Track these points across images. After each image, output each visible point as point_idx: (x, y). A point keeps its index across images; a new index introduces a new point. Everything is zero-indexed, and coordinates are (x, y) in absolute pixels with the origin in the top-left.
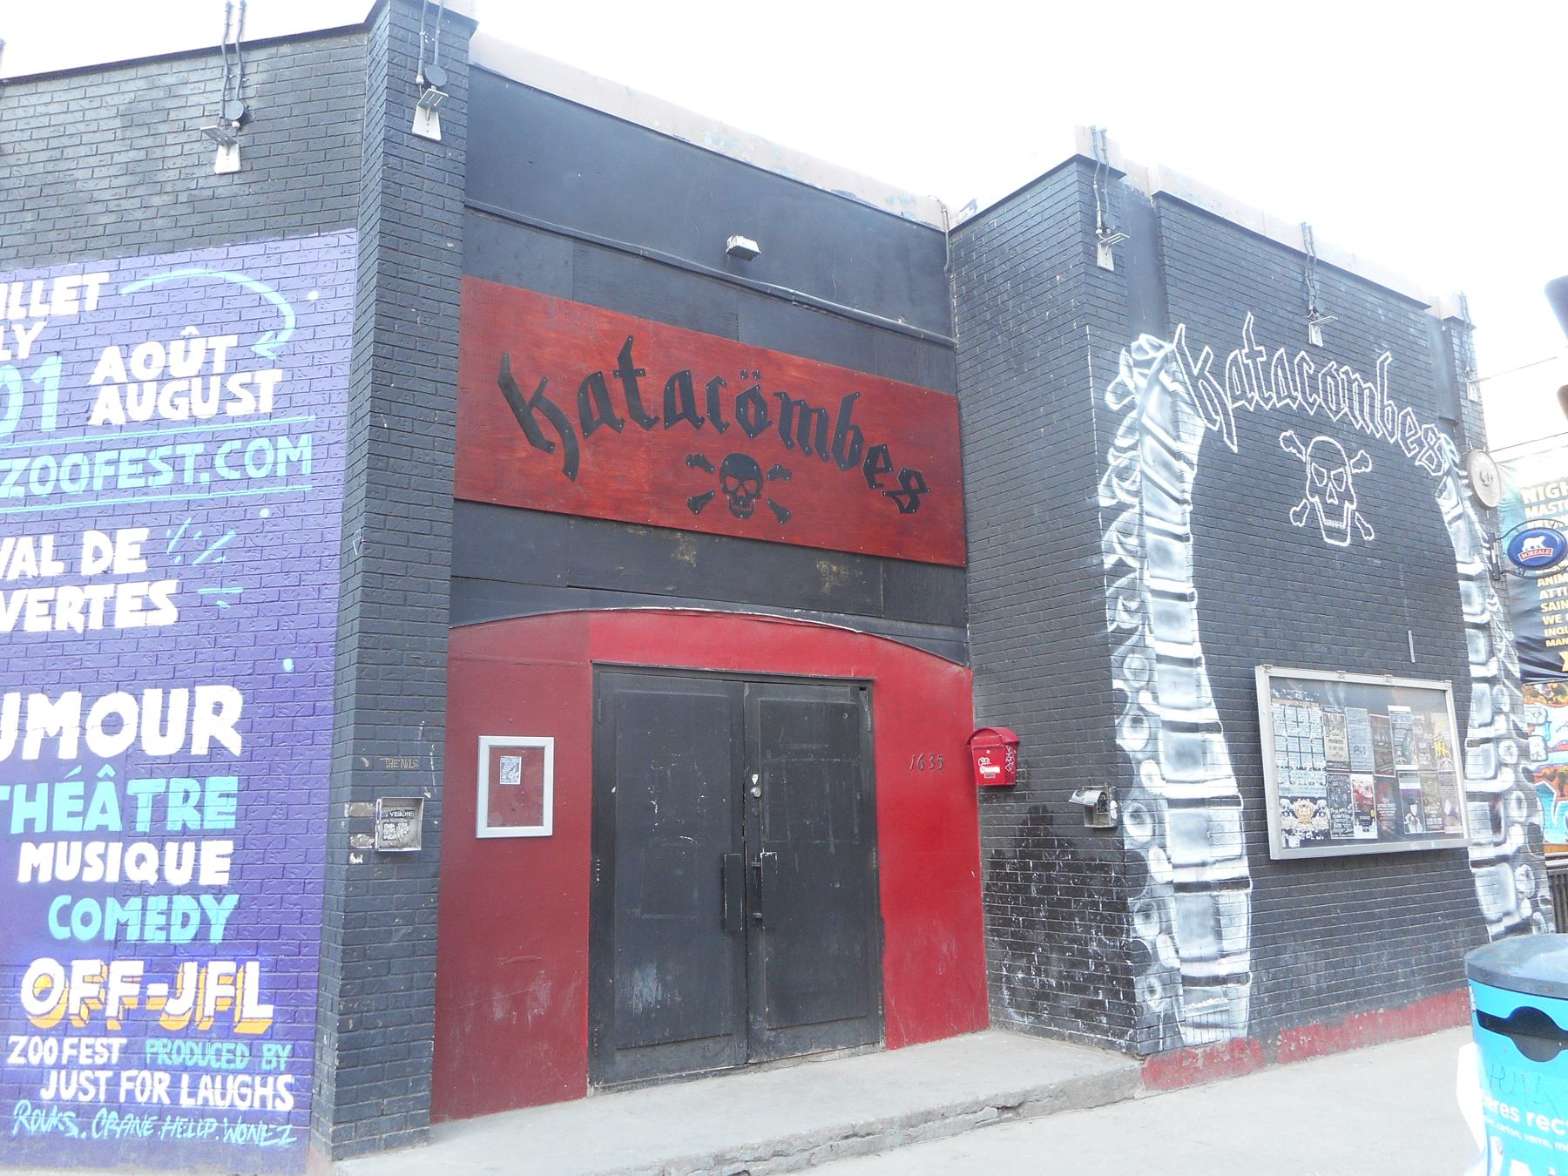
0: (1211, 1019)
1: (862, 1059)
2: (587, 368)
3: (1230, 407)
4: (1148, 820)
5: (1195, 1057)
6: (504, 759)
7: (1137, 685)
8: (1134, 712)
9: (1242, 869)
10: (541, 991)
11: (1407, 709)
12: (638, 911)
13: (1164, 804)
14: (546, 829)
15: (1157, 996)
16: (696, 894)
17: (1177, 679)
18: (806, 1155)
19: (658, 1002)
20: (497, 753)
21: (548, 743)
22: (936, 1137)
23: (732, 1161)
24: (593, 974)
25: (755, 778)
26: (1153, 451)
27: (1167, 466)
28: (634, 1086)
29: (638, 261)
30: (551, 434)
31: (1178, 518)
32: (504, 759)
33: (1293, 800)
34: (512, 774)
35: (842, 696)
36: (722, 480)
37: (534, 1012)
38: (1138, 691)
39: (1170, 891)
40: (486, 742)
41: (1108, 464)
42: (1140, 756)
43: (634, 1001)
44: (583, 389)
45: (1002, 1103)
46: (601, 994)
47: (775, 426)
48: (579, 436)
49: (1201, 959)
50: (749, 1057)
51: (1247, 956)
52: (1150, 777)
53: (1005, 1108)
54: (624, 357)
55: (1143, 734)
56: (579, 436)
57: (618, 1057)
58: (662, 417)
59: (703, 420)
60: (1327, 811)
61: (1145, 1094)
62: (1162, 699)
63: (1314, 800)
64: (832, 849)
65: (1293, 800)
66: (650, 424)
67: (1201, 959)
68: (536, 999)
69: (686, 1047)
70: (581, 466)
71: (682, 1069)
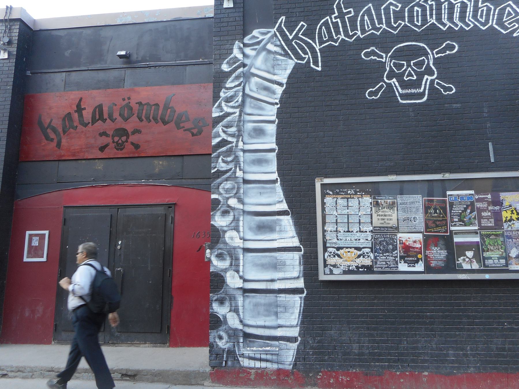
0: (263, 356)
2: (67, 112)
3: (317, 48)
4: (228, 258)
5: (249, 373)
6: (34, 238)
7: (227, 196)
8: (224, 208)
9: (300, 284)
10: (40, 309)
11: (472, 192)
13: (240, 252)
14: (44, 259)
15: (224, 341)
17: (262, 191)
18: (31, 374)
20: (31, 236)
21: (47, 232)
25: (120, 242)
26: (256, 83)
27: (266, 89)
29: (205, 66)
30: (52, 135)
31: (271, 113)
32: (34, 238)
33: (338, 249)
34: (35, 242)
35: (160, 211)
36: (113, 139)
38: (228, 198)
39: (240, 292)
40: (28, 233)
41: (220, 97)
42: (225, 229)
44: (64, 119)
45: (124, 372)
47: (135, 115)
48: (62, 135)
49: (264, 327)
51: (298, 329)
52: (232, 238)
53: (126, 375)
54: (79, 106)
55: (229, 218)
56: (62, 135)
58: (91, 122)
59: (106, 119)
60: (372, 255)
61: (211, 384)
62: (247, 200)
63: (358, 249)
64: (149, 269)
65: (338, 249)
66: (86, 125)
67: (264, 327)
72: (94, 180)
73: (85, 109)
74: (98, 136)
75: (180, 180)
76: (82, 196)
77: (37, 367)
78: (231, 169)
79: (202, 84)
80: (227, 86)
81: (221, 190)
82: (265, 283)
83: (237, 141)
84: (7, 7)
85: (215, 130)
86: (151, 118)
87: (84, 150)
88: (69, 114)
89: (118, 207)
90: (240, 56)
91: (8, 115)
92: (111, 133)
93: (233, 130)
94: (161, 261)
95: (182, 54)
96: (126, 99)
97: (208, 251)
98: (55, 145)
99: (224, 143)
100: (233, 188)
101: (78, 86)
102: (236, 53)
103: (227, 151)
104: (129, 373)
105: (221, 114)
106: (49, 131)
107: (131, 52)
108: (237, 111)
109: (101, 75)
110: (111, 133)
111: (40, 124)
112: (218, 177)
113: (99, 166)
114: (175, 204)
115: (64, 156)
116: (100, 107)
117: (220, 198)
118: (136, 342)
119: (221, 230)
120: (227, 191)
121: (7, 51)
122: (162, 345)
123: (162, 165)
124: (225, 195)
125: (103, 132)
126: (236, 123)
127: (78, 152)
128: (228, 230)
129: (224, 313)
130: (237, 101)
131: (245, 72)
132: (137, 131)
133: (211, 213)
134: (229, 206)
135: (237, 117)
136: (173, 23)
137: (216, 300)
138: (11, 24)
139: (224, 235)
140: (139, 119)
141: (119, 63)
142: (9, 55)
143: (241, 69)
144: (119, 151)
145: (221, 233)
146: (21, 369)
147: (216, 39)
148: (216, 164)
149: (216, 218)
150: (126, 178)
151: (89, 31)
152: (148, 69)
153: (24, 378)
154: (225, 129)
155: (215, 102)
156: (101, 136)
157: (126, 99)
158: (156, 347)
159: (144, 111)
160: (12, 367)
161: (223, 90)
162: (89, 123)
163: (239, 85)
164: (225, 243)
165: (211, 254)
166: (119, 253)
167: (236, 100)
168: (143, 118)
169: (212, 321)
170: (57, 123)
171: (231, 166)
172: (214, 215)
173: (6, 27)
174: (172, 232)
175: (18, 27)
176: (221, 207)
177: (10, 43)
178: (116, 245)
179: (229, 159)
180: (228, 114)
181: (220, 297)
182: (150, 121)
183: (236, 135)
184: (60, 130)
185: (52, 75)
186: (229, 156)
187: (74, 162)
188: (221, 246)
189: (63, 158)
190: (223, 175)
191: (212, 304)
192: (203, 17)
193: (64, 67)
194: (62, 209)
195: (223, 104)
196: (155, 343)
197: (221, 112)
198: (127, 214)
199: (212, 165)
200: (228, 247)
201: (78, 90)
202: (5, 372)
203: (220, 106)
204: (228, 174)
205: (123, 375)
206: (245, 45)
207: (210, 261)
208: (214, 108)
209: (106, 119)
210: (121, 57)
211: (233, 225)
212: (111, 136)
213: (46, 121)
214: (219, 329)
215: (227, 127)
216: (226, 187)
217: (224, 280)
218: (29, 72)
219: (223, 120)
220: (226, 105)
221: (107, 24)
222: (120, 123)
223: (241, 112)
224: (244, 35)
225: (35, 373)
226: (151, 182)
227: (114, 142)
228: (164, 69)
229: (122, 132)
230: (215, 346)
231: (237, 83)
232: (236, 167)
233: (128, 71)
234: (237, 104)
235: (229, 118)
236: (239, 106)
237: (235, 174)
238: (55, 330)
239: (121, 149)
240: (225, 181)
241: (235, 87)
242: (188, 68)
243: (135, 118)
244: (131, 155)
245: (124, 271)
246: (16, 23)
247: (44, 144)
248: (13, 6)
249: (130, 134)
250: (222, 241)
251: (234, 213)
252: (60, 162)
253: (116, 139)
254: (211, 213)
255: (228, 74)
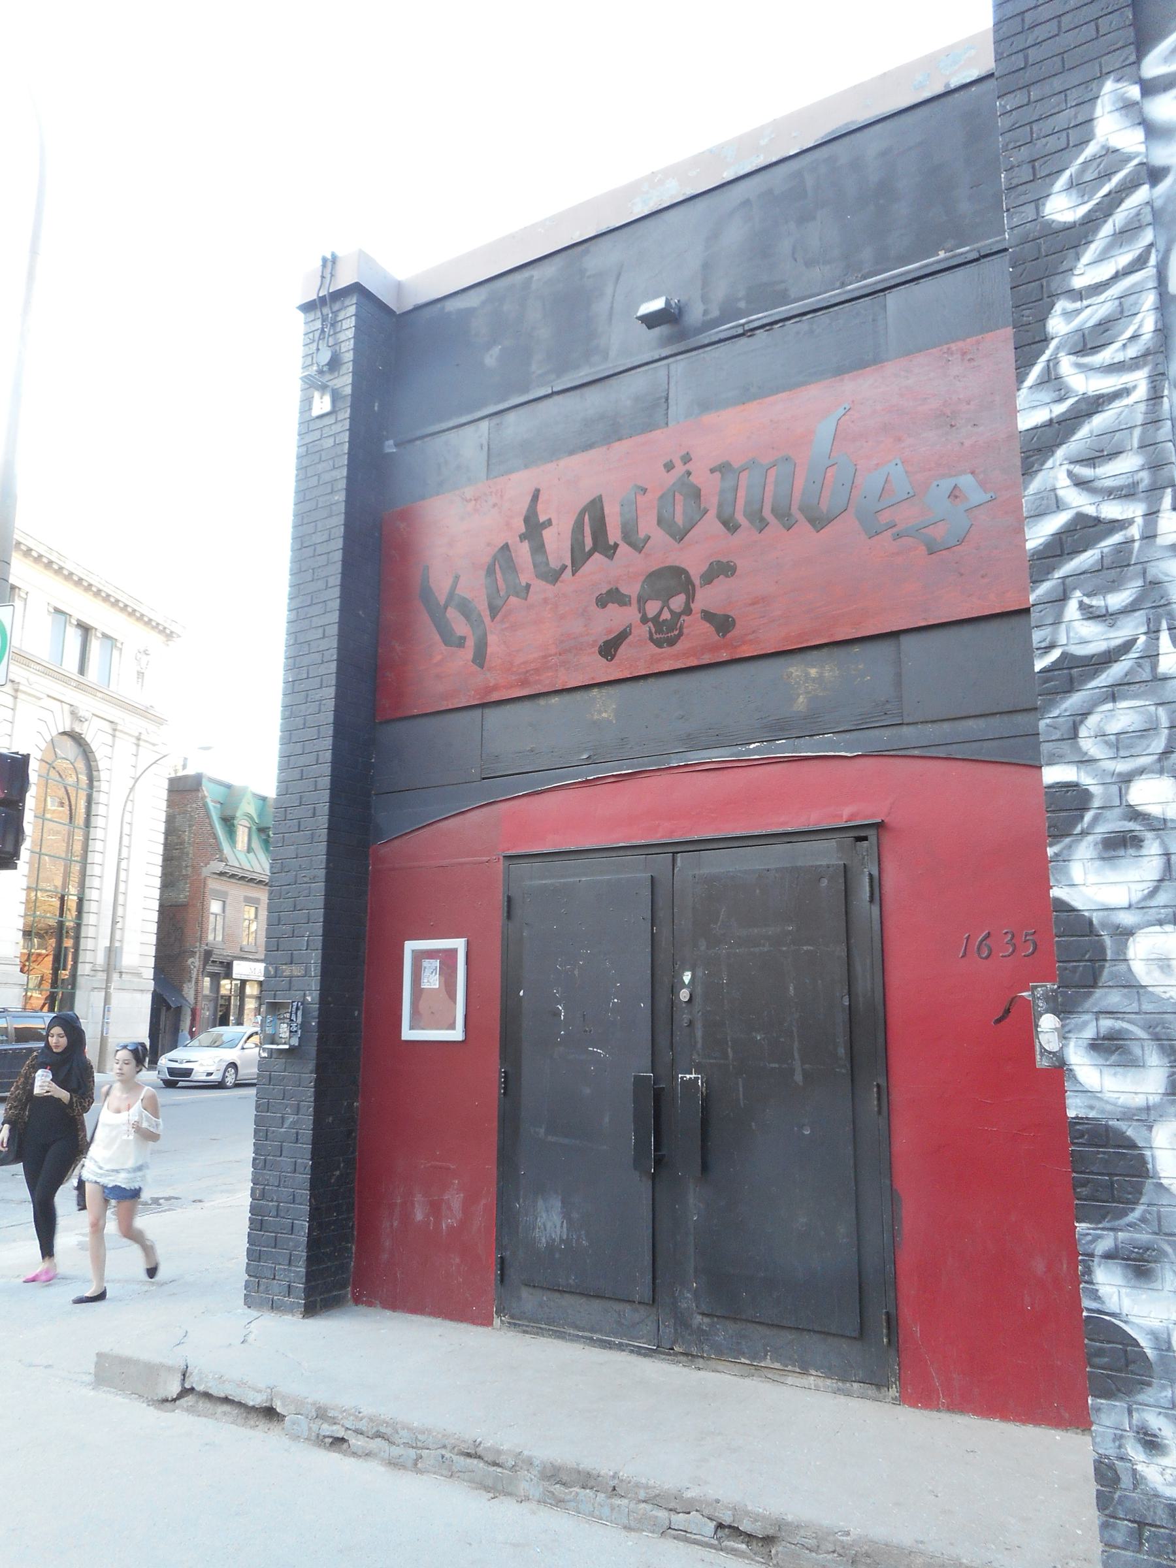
1: (854, 1404)
6: (426, 963)
7: (1122, 767)
8: (1113, 824)
10: (455, 1200)
12: (542, 1131)
14: (457, 1034)
16: (607, 1120)
18: (412, 1453)
19: (562, 1240)
20: (419, 956)
22: (594, 1516)
23: (334, 1421)
24: (501, 1195)
25: (687, 977)
28: (540, 1332)
29: (960, 273)
30: (461, 627)
32: (426, 963)
34: (432, 980)
36: (642, 609)
37: (447, 1222)
38: (1126, 779)
40: (410, 946)
42: (1127, 919)
43: (537, 1234)
44: (490, 571)
45: (727, 1519)
46: (507, 1220)
50: (674, 1342)
53: (735, 1531)
57: (525, 1293)
58: (568, 563)
59: (616, 546)
64: (798, 1078)
66: (554, 576)
68: (449, 1208)
69: (597, 1304)
70: (489, 650)
71: (593, 1330)
72: (590, 761)
73: (549, 523)
74: (593, 607)
75: (894, 730)
76: (563, 818)
77: (429, 1431)
78: (1128, 646)
79: (953, 347)
80: (1078, 282)
81: (1088, 745)
82: (780, 848)
83: (1152, 515)
84: (325, 260)
85: (1036, 484)
86: (767, 513)
87: (554, 660)
88: (506, 547)
89: (675, 849)
90: (1131, 140)
91: (338, 582)
92: (632, 589)
93: (1127, 465)
94: (842, 1051)
95: (867, 254)
96: (678, 463)
97: (1048, 1022)
98: (470, 656)
99: (1085, 530)
100: (1148, 731)
101: (532, 453)
102: (1111, 129)
103: (1101, 568)
104: (746, 1526)
105: (1060, 409)
106: (452, 614)
107: (684, 299)
108: (1139, 380)
109: (594, 399)
110: (632, 589)
111: (427, 594)
112: (1070, 687)
113: (604, 707)
114: (879, 826)
115: (496, 688)
116: (595, 511)
117: (1086, 779)
118: (767, 1363)
119: (1104, 925)
120: (1119, 743)
121: (329, 389)
122: (871, 1391)
123: (820, 679)
124: (1110, 765)
125: (609, 592)
126: (1137, 432)
127: (537, 671)
128: (1140, 927)
129: (1155, 1324)
130: (1135, 337)
131: (1158, 204)
132: (721, 569)
133: (1050, 851)
134: (1135, 814)
135: (1142, 407)
136: (824, 152)
137: (1109, 1256)
138: (336, 307)
139: (1122, 949)
140: (725, 523)
141: (648, 342)
142: (334, 402)
143: (1142, 194)
144: (667, 650)
145: (1108, 941)
146: (383, 1430)
147: (1009, 103)
148: (1055, 633)
149: (1077, 870)
150: (692, 742)
151: (549, 270)
152: (744, 340)
153: (394, 1464)
154: (1085, 472)
155: (1023, 365)
156: (604, 606)
157: (678, 463)
158: (848, 1394)
159: (741, 494)
160: (358, 1415)
161: (1061, 305)
162: (564, 567)
163: (1139, 263)
164: (1132, 986)
165: (1064, 1036)
166: (686, 1017)
167: (1128, 333)
168: (740, 518)
169: (1100, 1353)
170: (474, 588)
171: (1132, 628)
172: (1063, 859)
173: (324, 319)
174: (877, 938)
175: (352, 310)
176: (1096, 819)
177: (334, 364)
178: (674, 990)
179: (1116, 600)
180: (1094, 404)
181: (1132, 1242)
182: (762, 524)
183: (1142, 486)
184: (482, 606)
185: (451, 436)
186: (1114, 586)
187: (527, 706)
188: (1113, 998)
189: (495, 696)
190: (1094, 674)
191: (1089, 1271)
192: (939, 89)
193: (483, 404)
194: (501, 865)
195: (1066, 365)
196: (842, 1374)
197: (1061, 400)
198: (705, 871)
199: (1037, 636)
200: (1147, 1007)
201: (526, 467)
202: (341, 1433)
203: (1051, 378)
204: (1117, 671)
205: (720, 1526)
206: (1150, 88)
207: (1060, 1071)
208: (1023, 392)
209: (616, 546)
210: (651, 321)
211: (1162, 898)
212: (634, 601)
213: (441, 584)
214: (1141, 1397)
215: (1091, 460)
216: (1114, 727)
217: (1142, 1160)
218: (391, 442)
219: (1072, 431)
220: (1078, 365)
221: (603, 229)
222: (663, 551)
223: (1157, 381)
224: (1142, 44)
225: (425, 1453)
226: (783, 748)
227: (644, 620)
228: (805, 324)
229: (673, 580)
230: (1126, 1481)
231: (1124, 259)
232: (1153, 633)
233: (679, 366)
234: (1132, 351)
235: (1098, 422)
236: (1146, 354)
237: (1154, 667)
238: (502, 1281)
239: (672, 642)
240: (1104, 701)
241: (1117, 277)
242: (891, 298)
243: (710, 525)
244: (706, 659)
245: (707, 1082)
246: (347, 302)
247: (439, 657)
248: (339, 254)
249: (697, 582)
250: (1114, 976)
251: (1163, 844)
252: (487, 711)
253: (652, 608)
254: (1050, 851)
255: (1076, 236)
